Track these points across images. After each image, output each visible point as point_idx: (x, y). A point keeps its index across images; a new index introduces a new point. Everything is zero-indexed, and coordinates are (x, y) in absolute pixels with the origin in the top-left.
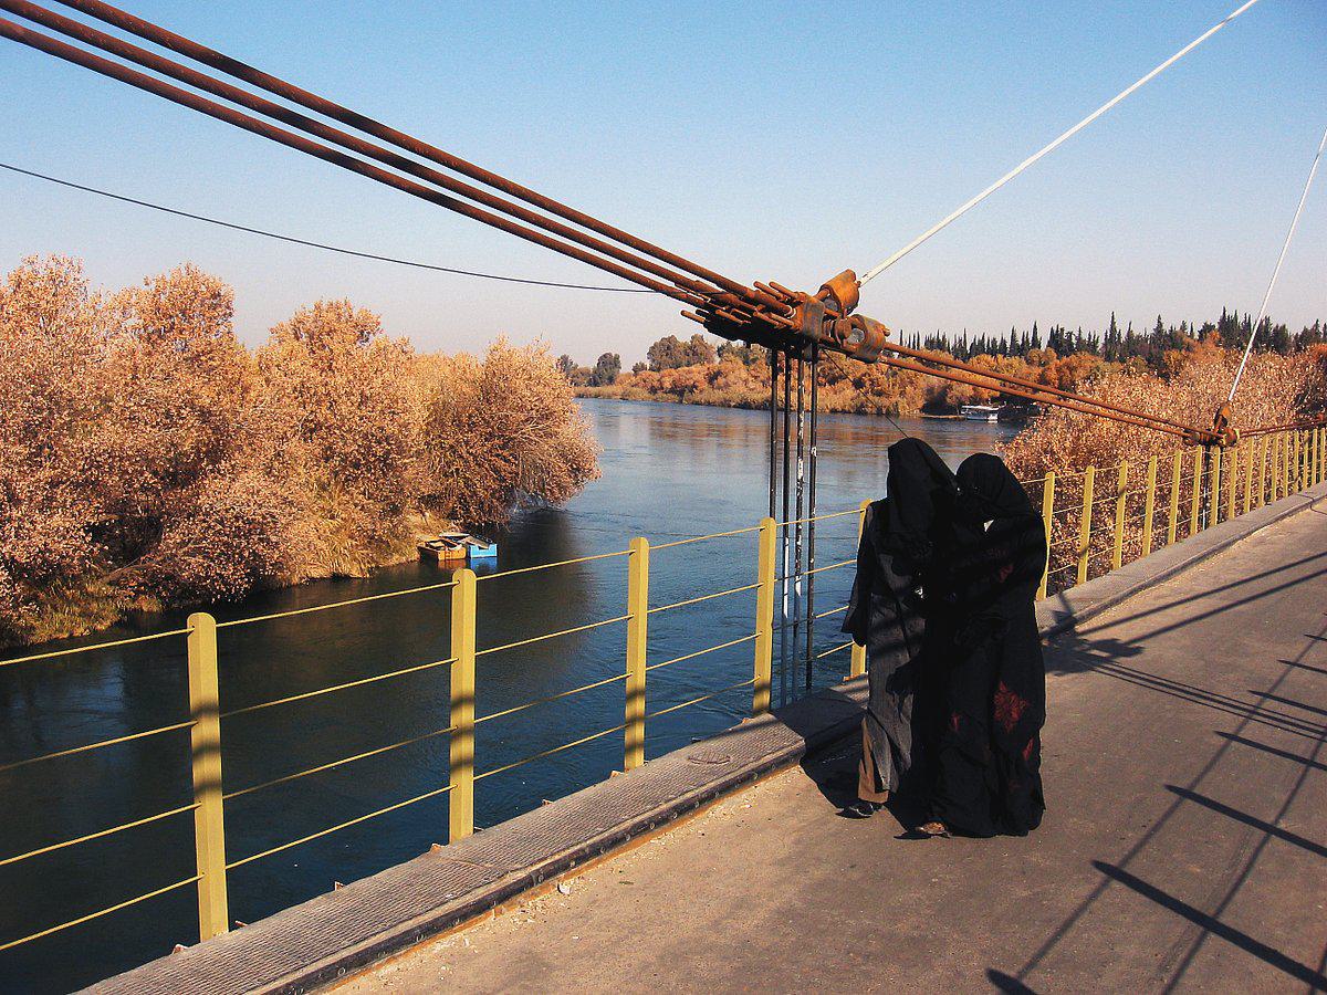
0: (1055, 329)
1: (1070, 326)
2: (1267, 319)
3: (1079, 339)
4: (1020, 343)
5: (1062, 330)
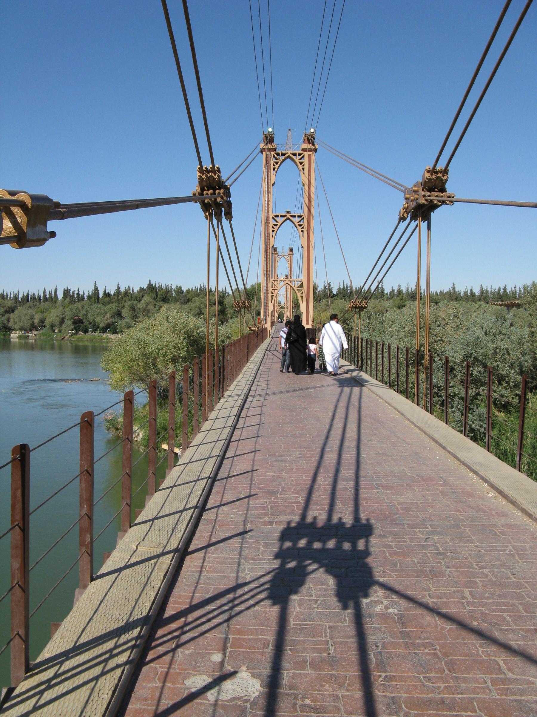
0: (66, 289)
1: (73, 288)
2: (177, 286)
3: (78, 294)
4: (48, 296)
5: (70, 290)
